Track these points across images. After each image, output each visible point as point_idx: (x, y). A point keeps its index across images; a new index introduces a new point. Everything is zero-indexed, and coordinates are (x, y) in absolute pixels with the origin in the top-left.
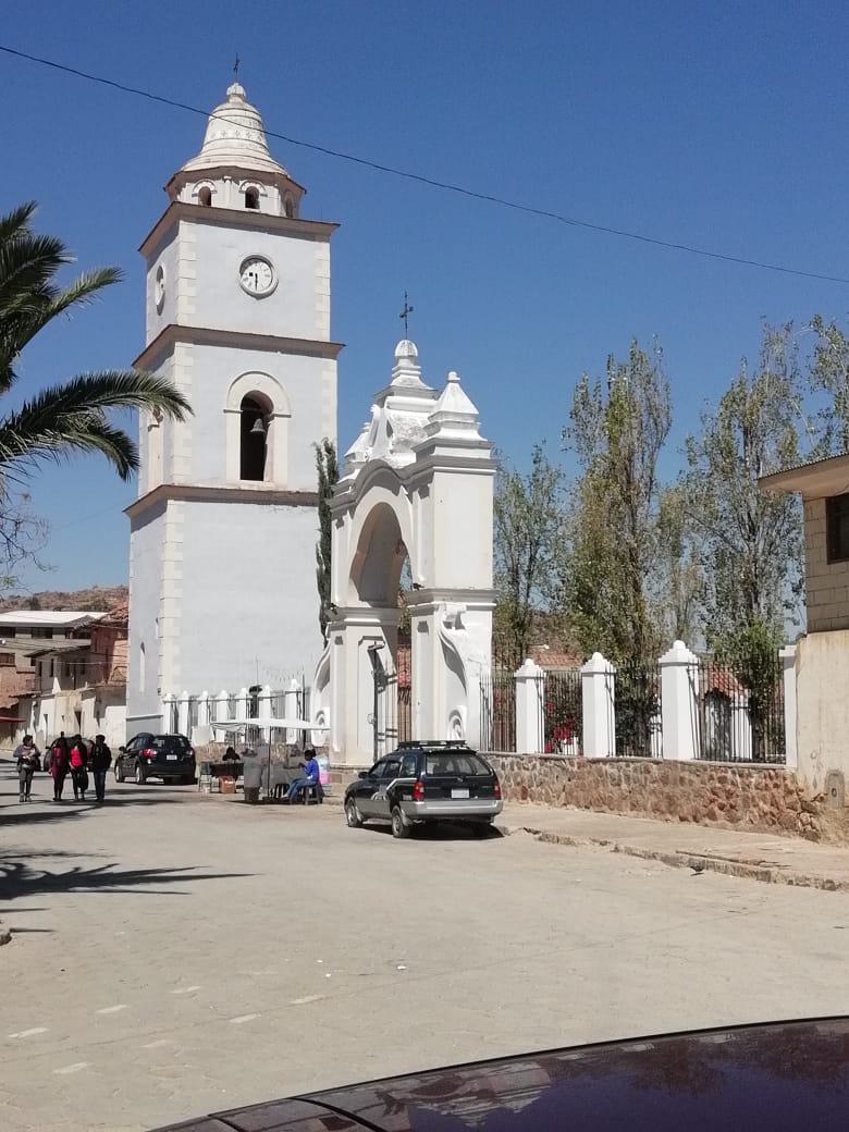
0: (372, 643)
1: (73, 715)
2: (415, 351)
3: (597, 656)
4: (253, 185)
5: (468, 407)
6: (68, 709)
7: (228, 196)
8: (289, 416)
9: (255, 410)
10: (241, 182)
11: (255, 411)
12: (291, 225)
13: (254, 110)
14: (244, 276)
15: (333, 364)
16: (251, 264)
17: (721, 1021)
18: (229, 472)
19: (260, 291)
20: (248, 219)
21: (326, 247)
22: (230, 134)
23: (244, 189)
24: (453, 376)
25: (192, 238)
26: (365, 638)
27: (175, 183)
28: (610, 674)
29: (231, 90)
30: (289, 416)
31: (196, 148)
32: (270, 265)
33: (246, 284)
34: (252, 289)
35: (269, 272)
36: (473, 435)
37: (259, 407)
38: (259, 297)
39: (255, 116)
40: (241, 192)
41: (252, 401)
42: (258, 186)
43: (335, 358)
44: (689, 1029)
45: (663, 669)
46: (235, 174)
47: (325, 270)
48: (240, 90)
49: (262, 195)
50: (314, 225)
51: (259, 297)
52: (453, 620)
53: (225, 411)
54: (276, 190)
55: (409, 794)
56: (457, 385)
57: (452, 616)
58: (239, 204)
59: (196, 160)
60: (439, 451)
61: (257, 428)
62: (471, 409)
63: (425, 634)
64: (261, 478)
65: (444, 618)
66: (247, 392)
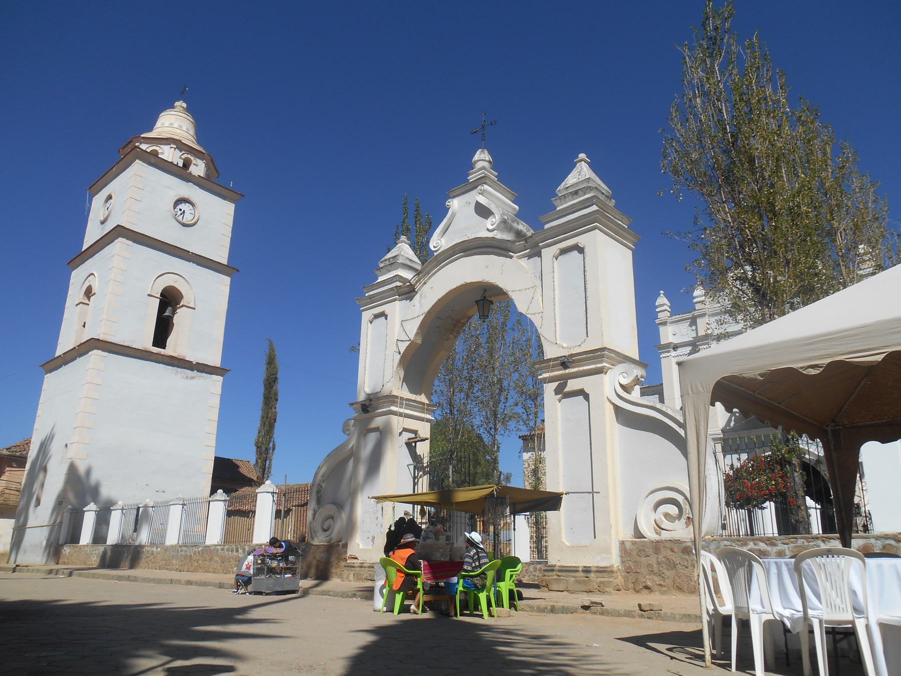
4: (189, 156)
7: (168, 153)
10: (183, 152)
15: (220, 379)
16: (181, 203)
18: (145, 339)
19: (184, 221)
20: (182, 172)
21: (222, 378)
22: (176, 125)
23: (183, 157)
26: (405, 430)
28: (276, 493)
29: (177, 104)
30: (194, 309)
31: (150, 127)
32: (193, 205)
35: (192, 212)
40: (180, 158)
42: (192, 158)
43: (222, 376)
45: (85, 513)
46: (179, 145)
47: (226, 290)
49: (194, 164)
53: (149, 295)
55: (137, 142)
61: (167, 313)
63: (565, 499)
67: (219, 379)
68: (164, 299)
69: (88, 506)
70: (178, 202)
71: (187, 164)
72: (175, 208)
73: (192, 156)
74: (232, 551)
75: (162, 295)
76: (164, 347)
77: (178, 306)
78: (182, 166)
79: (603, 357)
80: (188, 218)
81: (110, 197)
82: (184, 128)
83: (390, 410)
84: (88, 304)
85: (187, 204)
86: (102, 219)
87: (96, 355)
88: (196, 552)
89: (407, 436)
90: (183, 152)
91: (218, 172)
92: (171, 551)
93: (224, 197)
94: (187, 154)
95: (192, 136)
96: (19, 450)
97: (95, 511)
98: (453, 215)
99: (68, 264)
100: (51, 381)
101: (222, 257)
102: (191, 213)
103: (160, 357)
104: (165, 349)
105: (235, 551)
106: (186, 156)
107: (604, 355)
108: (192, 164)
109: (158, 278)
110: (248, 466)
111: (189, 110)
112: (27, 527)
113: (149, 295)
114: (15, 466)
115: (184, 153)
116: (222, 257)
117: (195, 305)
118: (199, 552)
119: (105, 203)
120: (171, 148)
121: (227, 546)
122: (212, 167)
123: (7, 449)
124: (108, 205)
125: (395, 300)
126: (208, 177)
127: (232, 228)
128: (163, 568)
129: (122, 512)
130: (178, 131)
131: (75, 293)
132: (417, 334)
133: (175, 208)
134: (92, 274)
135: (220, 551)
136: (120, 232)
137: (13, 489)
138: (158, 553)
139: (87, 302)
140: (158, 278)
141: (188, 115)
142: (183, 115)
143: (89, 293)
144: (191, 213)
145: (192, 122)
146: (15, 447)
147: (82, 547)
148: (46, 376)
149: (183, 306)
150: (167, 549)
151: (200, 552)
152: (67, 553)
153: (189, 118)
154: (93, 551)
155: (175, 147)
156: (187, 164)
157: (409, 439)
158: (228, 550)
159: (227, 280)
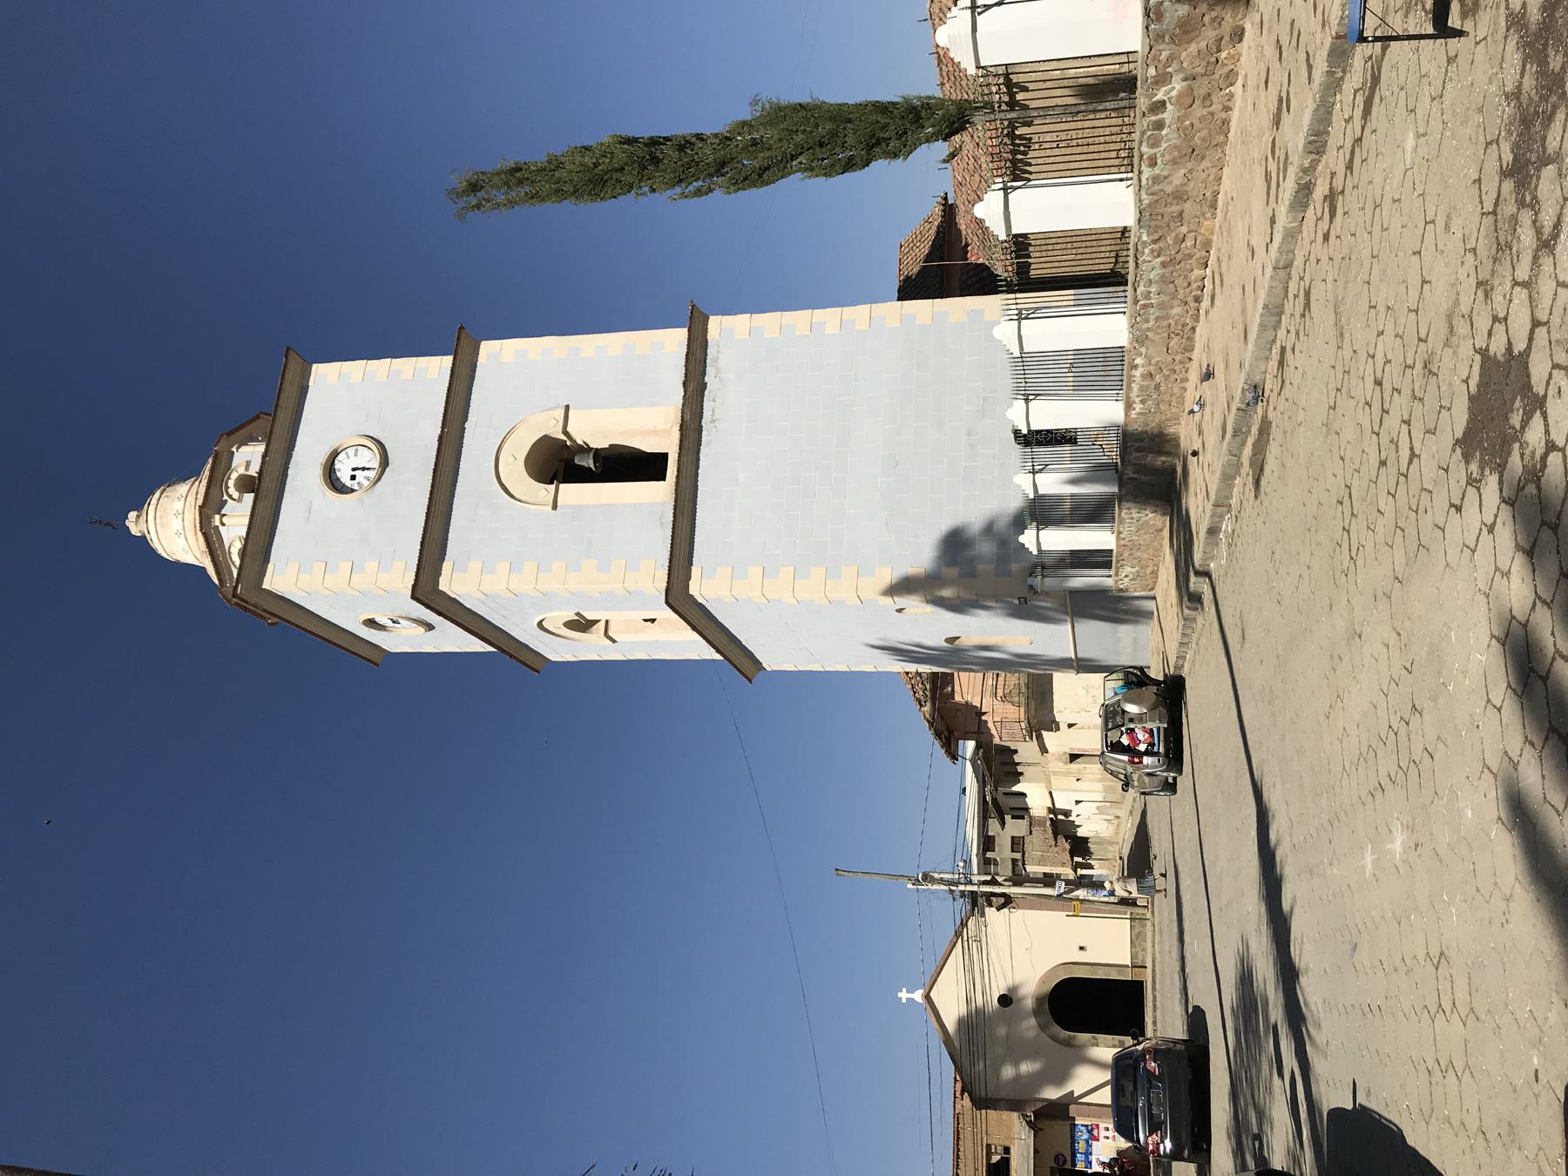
1: (1074, 766)
3: (1022, 539)
4: (231, 483)
6: (1068, 774)
7: (235, 524)
8: (567, 407)
10: (225, 497)
14: (356, 487)
15: (713, 322)
16: (338, 479)
17: (1171, 921)
18: (657, 495)
19: (375, 464)
23: (236, 495)
25: (293, 568)
29: (135, 530)
30: (567, 407)
32: (335, 454)
34: (372, 474)
35: (351, 451)
38: (385, 462)
40: (240, 500)
42: (234, 476)
44: (1238, 727)
45: (1043, 549)
46: (211, 507)
47: (354, 370)
49: (247, 468)
51: (385, 462)
53: (555, 507)
54: (243, 449)
61: (589, 463)
64: (665, 456)
67: (715, 324)
68: (560, 476)
69: (1030, 550)
70: (337, 485)
72: (353, 491)
73: (229, 478)
74: (1159, 125)
76: (664, 457)
77: (568, 443)
80: (370, 458)
81: (371, 623)
84: (607, 622)
85: (336, 467)
86: (421, 630)
87: (698, 588)
88: (1152, 251)
90: (225, 497)
91: (258, 417)
92: (1145, 326)
93: (303, 391)
95: (192, 485)
96: (920, 685)
97: (1038, 530)
99: (538, 672)
100: (775, 656)
101: (438, 367)
103: (684, 459)
104: (667, 454)
105: (1160, 116)
106: (232, 490)
108: (248, 473)
110: (912, 245)
111: (139, 504)
112: (1073, 657)
113: (555, 507)
114: (950, 689)
116: (438, 367)
118: (1155, 242)
119: (386, 630)
120: (223, 524)
121: (1144, 149)
122: (243, 433)
123: (921, 706)
124: (390, 624)
128: (1190, 339)
129: (1040, 471)
131: (590, 648)
133: (353, 491)
134: (540, 624)
135: (1157, 171)
136: (426, 590)
137: (995, 683)
138: (1149, 359)
139: (602, 625)
141: (149, 504)
142: (152, 507)
143: (581, 625)
144: (356, 455)
145: (162, 493)
146: (915, 693)
147: (1122, 542)
148: (768, 669)
149: (566, 433)
150: (1139, 339)
151: (1156, 236)
152: (1134, 570)
153: (154, 501)
154: (1132, 518)
155: (217, 517)
156: (247, 484)
158: (1155, 143)
159: (488, 348)
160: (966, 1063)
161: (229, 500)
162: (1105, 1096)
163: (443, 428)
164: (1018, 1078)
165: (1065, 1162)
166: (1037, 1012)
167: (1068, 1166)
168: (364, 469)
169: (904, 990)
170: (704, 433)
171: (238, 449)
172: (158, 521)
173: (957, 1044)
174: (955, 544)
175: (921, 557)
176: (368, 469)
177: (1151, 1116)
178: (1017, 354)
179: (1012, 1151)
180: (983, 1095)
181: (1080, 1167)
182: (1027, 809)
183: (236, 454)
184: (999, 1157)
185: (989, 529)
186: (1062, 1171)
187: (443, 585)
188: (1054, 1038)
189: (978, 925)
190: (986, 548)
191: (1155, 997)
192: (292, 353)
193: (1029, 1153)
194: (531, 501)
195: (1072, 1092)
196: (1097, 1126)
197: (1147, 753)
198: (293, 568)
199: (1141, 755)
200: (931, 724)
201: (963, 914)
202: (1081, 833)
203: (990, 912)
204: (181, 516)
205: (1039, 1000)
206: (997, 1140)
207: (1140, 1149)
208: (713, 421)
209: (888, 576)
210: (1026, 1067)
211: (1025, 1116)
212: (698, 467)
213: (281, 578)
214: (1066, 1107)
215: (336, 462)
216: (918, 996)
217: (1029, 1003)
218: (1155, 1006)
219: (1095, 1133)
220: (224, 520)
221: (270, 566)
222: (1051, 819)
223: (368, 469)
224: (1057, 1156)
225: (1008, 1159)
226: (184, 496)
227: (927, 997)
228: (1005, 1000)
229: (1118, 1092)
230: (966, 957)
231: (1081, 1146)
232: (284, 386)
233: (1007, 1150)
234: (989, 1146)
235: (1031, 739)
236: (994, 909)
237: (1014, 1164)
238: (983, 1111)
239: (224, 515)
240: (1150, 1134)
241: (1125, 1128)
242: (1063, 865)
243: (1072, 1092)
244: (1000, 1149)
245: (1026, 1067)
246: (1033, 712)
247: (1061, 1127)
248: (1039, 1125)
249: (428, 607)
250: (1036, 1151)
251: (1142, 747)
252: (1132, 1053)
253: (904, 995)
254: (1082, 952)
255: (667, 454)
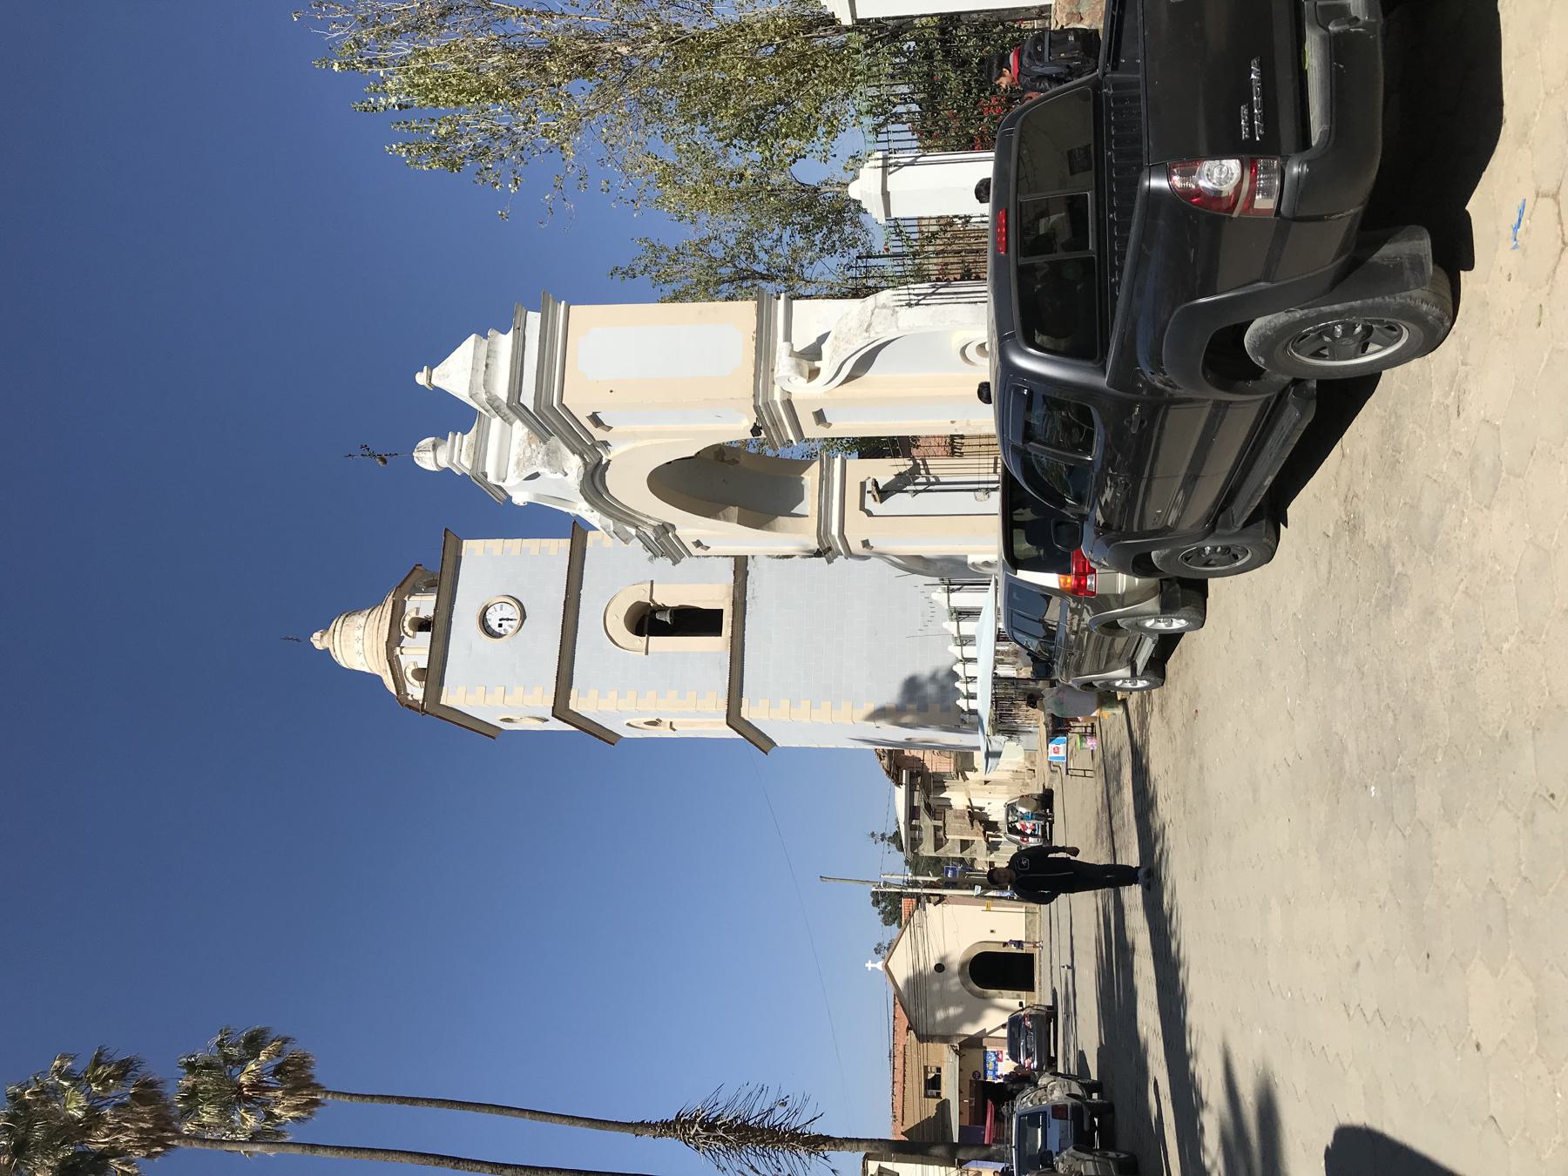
0: (868, 497)
1: (987, 786)
2: (428, 441)
4: (406, 624)
5: (467, 349)
6: (983, 790)
7: (416, 651)
8: (652, 582)
9: (647, 618)
10: (403, 634)
11: (646, 621)
12: (443, 581)
13: (335, 622)
14: (503, 633)
16: (489, 626)
18: (711, 649)
19: (517, 615)
20: (436, 627)
21: (468, 545)
23: (411, 633)
24: (421, 379)
25: (461, 690)
26: (862, 508)
27: (412, 706)
29: (318, 646)
30: (652, 582)
32: (486, 609)
33: (510, 631)
34: (515, 624)
36: (505, 342)
37: (644, 617)
38: (524, 616)
39: (341, 620)
40: (414, 637)
41: (638, 624)
42: (408, 619)
46: (394, 640)
47: (495, 545)
48: (317, 635)
49: (417, 613)
50: (446, 557)
51: (524, 616)
52: (806, 366)
53: (647, 653)
54: (412, 598)
56: (435, 371)
57: (798, 365)
58: (425, 637)
59: (384, 678)
60: (528, 399)
61: (667, 618)
62: (470, 343)
65: (802, 381)
66: (625, 629)
68: (646, 628)
70: (489, 630)
71: (422, 625)
72: (500, 636)
73: (404, 620)
75: (643, 635)
77: (652, 605)
78: (430, 633)
79: (768, 403)
80: (512, 612)
82: (359, 633)
83: (839, 537)
87: (746, 713)
89: (870, 503)
90: (403, 634)
94: (403, 627)
98: (538, 496)
102: (501, 609)
104: (722, 610)
106: (407, 629)
107: (764, 404)
109: (617, 645)
111: (325, 626)
113: (647, 653)
115: (404, 631)
117: (644, 582)
120: (402, 654)
123: (881, 759)
125: (676, 537)
126: (432, 585)
127: (505, 538)
129: (965, 645)
130: (367, 643)
132: (727, 519)
133: (500, 636)
140: (617, 645)
144: (501, 609)
155: (398, 649)
156: (422, 625)
157: (875, 500)
160: (912, 1008)
161: (406, 637)
162: (1004, 1033)
163: (566, 595)
164: (947, 1019)
165: (979, 1077)
166: (961, 972)
167: (982, 1079)
168: (508, 619)
169: (870, 961)
170: (748, 606)
171: (409, 598)
172: (342, 643)
173: (906, 997)
174: (912, 686)
175: (891, 694)
176: (511, 620)
177: (1027, 1049)
178: (956, 635)
179: (942, 1070)
180: (925, 1033)
181: (989, 1079)
182: (951, 806)
183: (408, 603)
184: (933, 1075)
185: (933, 678)
186: (978, 1083)
187: (572, 706)
188: (971, 991)
189: (920, 915)
190: (931, 690)
191: (1040, 966)
192: (448, 533)
193: (955, 1068)
194: (630, 647)
195: (985, 1030)
196: (1002, 1052)
197: (1032, 835)
198: (461, 690)
199: (1028, 836)
200: (888, 773)
201: (911, 908)
202: (991, 819)
203: (929, 907)
204: (361, 641)
205: (963, 966)
206: (933, 1063)
207: (1021, 1067)
208: (753, 598)
209: (870, 707)
210: (952, 1011)
211: (952, 1046)
212: (744, 630)
213: (451, 697)
214: (981, 1040)
215: (487, 614)
216: (880, 965)
217: (956, 967)
218: (1040, 972)
219: (1000, 1056)
220: (403, 650)
221: (445, 688)
222: (969, 812)
223: (511, 620)
224: (974, 1073)
225: (940, 1076)
226: (363, 626)
227: (886, 967)
228: (940, 968)
229: (1010, 1033)
230: (913, 938)
231: (990, 1066)
232: (445, 557)
233: (939, 1070)
234: (926, 1068)
235: (958, 778)
236: (932, 905)
237: (943, 1079)
238: (925, 1044)
239: (403, 647)
240: (1027, 1058)
241: (1014, 1056)
242: (977, 835)
243: (985, 1030)
244: (934, 1070)
245: (952, 1011)
246: (959, 764)
247: (977, 1054)
248: (963, 1052)
249: (565, 721)
250: (960, 1070)
251: (1029, 831)
252: (1018, 1016)
253: (869, 965)
254: (992, 934)
255: (722, 610)
